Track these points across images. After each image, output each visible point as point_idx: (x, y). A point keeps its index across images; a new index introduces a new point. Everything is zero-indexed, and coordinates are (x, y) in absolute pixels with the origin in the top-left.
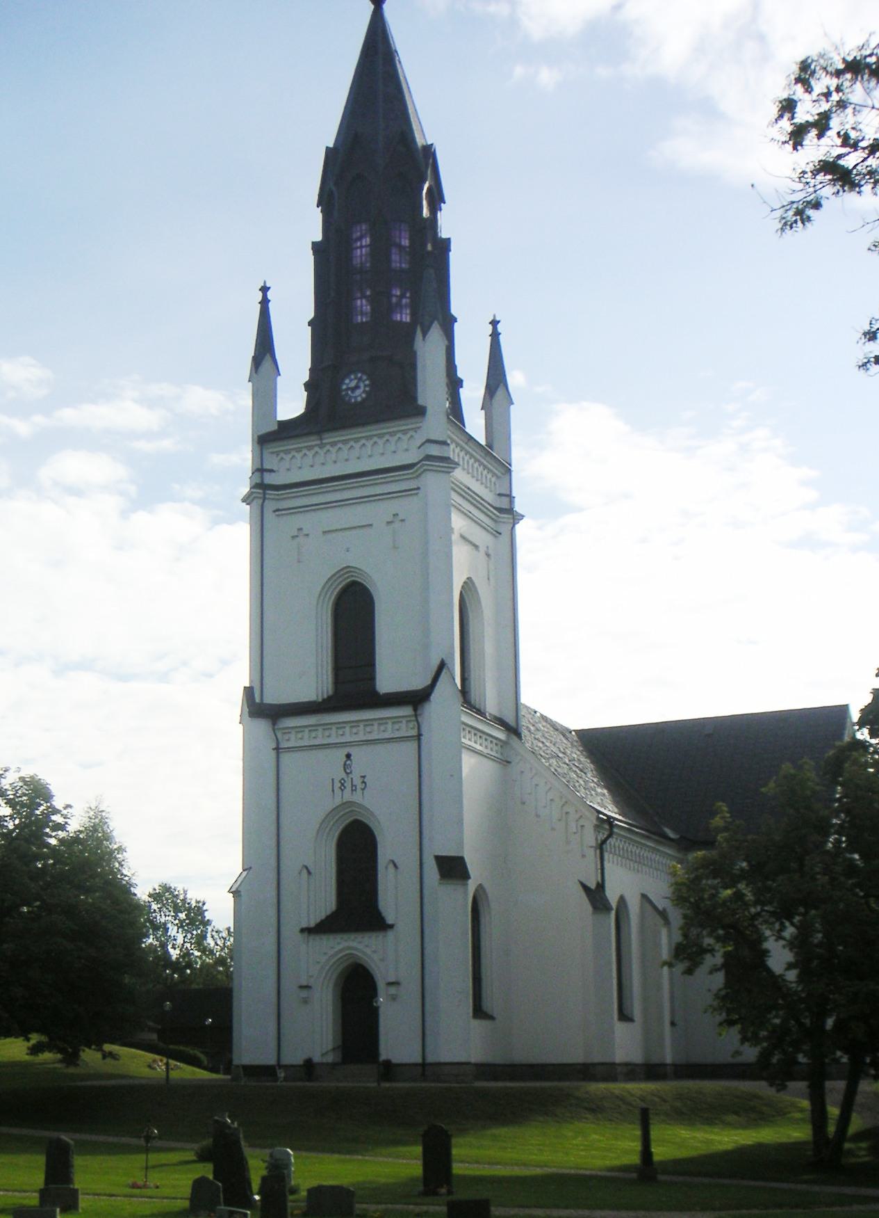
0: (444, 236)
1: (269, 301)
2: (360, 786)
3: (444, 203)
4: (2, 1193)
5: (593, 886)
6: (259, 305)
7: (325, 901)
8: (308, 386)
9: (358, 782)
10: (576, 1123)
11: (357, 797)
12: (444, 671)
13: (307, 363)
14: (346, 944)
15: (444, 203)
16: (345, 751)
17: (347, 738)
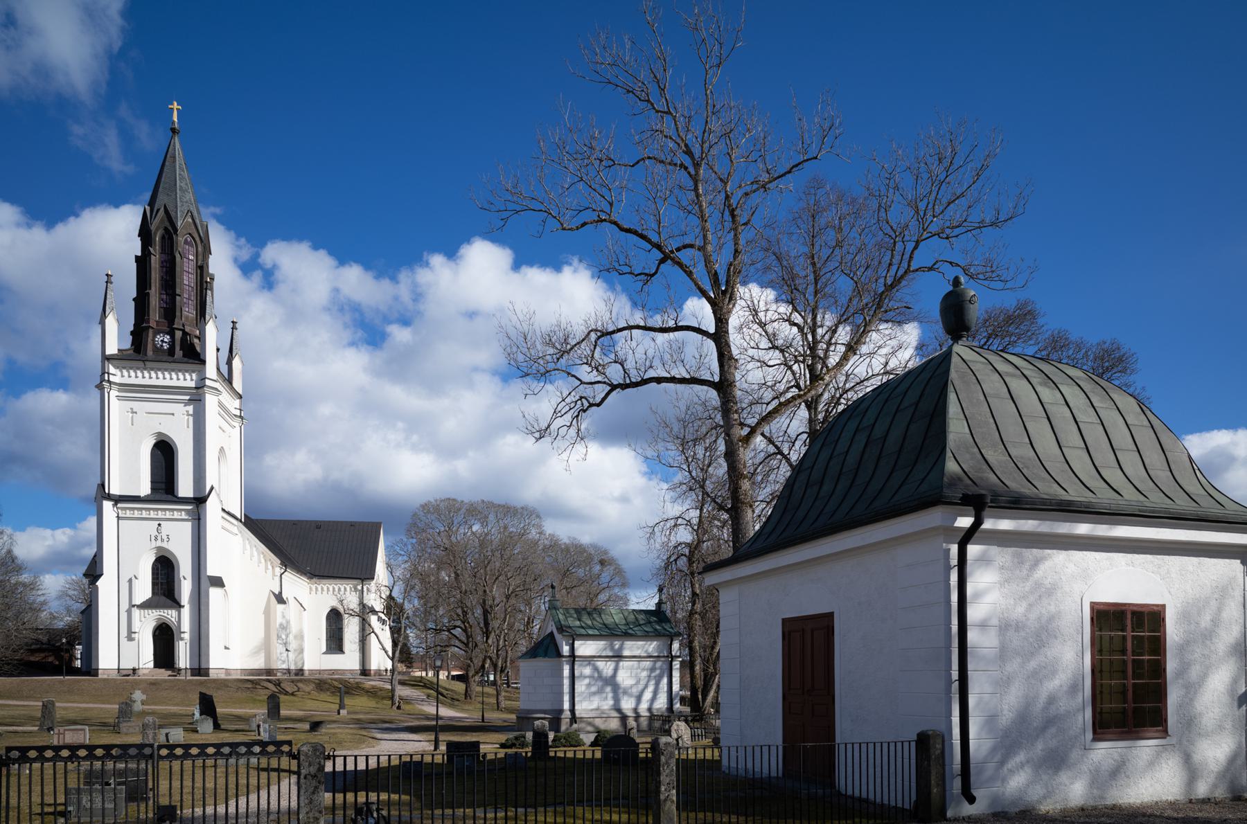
0: (116, 352)
1: (134, 300)
2: (166, 539)
3: (136, 257)
5: (277, 593)
6: (133, 302)
7: (144, 590)
8: (132, 333)
9: (165, 537)
10: (432, 500)
11: (165, 545)
12: (214, 490)
13: (133, 322)
14: (159, 613)
15: (136, 257)
16: (158, 522)
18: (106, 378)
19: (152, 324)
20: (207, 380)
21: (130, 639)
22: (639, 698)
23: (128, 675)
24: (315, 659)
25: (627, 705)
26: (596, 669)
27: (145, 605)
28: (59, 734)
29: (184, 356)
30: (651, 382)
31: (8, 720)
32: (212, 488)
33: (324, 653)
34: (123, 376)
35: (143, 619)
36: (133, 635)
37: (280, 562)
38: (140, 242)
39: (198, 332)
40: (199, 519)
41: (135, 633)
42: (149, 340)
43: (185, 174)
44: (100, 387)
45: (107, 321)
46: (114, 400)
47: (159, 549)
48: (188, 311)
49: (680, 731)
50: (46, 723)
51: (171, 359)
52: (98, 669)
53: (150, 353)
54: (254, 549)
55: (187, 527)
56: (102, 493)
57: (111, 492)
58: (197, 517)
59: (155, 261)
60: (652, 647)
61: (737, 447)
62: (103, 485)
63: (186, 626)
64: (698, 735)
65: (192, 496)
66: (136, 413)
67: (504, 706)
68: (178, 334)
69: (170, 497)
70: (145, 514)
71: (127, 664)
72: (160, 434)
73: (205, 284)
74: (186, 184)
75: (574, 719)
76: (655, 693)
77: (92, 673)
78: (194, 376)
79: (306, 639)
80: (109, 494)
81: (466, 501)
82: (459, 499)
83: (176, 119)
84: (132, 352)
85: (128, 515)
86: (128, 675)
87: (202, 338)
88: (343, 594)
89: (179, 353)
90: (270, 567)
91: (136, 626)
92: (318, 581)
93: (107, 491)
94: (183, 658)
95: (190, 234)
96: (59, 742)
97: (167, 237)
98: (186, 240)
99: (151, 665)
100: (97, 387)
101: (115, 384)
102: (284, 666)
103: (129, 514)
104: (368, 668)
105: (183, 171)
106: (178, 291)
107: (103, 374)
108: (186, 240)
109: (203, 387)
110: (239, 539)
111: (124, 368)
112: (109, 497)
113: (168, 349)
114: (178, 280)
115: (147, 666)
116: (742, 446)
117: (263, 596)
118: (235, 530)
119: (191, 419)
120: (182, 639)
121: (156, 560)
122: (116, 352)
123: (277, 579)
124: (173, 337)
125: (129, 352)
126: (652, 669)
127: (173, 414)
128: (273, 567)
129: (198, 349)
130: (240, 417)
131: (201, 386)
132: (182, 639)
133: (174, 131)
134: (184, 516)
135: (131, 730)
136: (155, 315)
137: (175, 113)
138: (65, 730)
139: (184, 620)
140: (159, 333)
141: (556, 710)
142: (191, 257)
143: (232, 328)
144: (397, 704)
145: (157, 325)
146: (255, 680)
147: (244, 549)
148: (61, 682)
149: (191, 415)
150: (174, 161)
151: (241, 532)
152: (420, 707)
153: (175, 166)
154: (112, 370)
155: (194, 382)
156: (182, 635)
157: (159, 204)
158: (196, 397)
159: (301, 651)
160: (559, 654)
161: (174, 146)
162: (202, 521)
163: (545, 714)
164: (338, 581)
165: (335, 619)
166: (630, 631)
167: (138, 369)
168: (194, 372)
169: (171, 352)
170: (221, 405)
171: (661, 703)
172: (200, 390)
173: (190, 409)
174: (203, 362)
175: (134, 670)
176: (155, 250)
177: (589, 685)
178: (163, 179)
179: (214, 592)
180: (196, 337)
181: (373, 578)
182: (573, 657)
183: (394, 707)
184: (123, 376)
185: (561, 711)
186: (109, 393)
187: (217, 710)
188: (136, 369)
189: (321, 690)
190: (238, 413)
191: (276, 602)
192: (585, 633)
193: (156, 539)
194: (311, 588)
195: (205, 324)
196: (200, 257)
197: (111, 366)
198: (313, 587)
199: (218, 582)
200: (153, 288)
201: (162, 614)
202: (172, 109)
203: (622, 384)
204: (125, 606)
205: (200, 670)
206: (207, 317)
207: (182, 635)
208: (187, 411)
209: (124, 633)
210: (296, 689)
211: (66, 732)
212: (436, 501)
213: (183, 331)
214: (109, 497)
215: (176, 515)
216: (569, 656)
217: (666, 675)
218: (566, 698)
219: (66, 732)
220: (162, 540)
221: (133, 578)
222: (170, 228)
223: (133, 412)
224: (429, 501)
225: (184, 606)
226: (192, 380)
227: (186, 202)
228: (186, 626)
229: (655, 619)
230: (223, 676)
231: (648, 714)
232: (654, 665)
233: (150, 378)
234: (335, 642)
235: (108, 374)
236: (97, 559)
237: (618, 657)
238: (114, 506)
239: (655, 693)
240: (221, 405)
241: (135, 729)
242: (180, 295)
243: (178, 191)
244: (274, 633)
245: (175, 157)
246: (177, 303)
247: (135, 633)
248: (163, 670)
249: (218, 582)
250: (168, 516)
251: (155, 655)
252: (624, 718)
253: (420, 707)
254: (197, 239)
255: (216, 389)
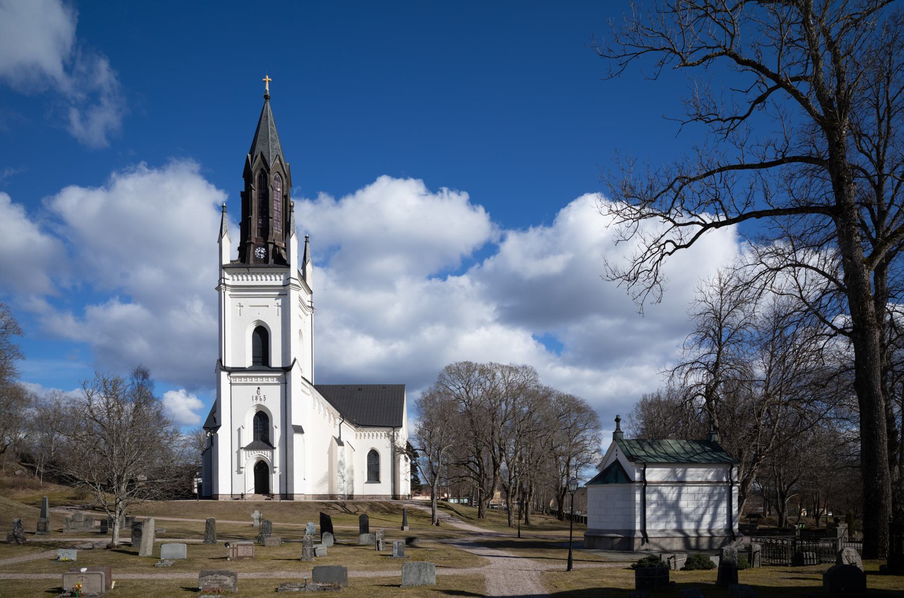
0: (229, 262)
2: (263, 399)
3: (242, 192)
4: (1, 583)
5: (337, 438)
7: (248, 437)
8: (239, 249)
9: (262, 397)
10: (453, 364)
11: (262, 403)
14: (259, 453)
15: (242, 192)
16: (258, 386)
17: (259, 382)
18: (223, 282)
19: (253, 241)
20: (291, 279)
21: (239, 472)
22: (699, 522)
23: (238, 499)
24: (362, 488)
25: (689, 527)
26: (660, 494)
27: (250, 448)
28: (233, 548)
29: (275, 263)
30: (750, 217)
31: (175, 533)
32: (295, 360)
33: (366, 483)
34: (233, 280)
35: (248, 458)
36: (241, 470)
37: (339, 414)
38: (244, 181)
39: (284, 245)
40: (286, 383)
41: (243, 468)
42: (251, 252)
43: (274, 129)
44: (219, 289)
45: (223, 240)
46: (228, 298)
47: (259, 406)
48: (277, 229)
49: (851, 558)
50: (209, 537)
51: (266, 265)
52: (293, 494)
53: (252, 262)
54: (321, 405)
55: (277, 390)
56: (221, 366)
57: (226, 365)
58: (284, 382)
59: (255, 194)
60: (709, 474)
61: (861, 269)
62: (221, 361)
63: (277, 463)
64: (810, 558)
65: (280, 366)
66: (242, 306)
67: (514, 523)
68: (271, 247)
69: (266, 368)
70: (249, 381)
71: (238, 491)
72: (259, 321)
73: (288, 207)
74: (275, 136)
75: (645, 538)
76: (714, 516)
77: (214, 497)
78: (282, 277)
79: (355, 472)
80: (225, 366)
81: (479, 364)
82: (474, 362)
83: (267, 89)
84: (239, 262)
85: (237, 382)
86: (238, 499)
87: (287, 249)
88: (379, 440)
89: (271, 261)
90: (332, 419)
91: (243, 463)
92: (361, 429)
93: (223, 365)
94: (275, 487)
95: (278, 172)
96: (233, 556)
97: (262, 176)
98: (276, 176)
99: (253, 491)
100: (216, 289)
101: (229, 286)
102: (342, 493)
103: (238, 381)
104: (397, 494)
105: (273, 126)
106: (270, 215)
107: (220, 279)
108: (275, 177)
109: (289, 284)
110: (311, 398)
111: (235, 274)
112: (225, 369)
113: (264, 258)
114: (270, 207)
115: (250, 492)
116: (867, 268)
117: (328, 440)
118: (308, 391)
119: (280, 308)
120: (275, 472)
121: (256, 414)
122: (229, 262)
123: (338, 427)
124: (267, 249)
125: (237, 262)
126: (711, 495)
127: (268, 306)
128: (334, 418)
129: (285, 257)
130: (312, 307)
131: (287, 284)
132: (275, 472)
133: (266, 97)
134: (276, 382)
135: (273, 544)
136: (255, 234)
137: (267, 83)
138: (238, 545)
139: (275, 458)
140: (257, 247)
141: (626, 531)
142: (279, 189)
143: (306, 242)
144: (436, 522)
145: (256, 241)
146: (328, 502)
147: (314, 405)
148: (196, 504)
149: (280, 306)
150: (267, 120)
151: (312, 393)
152: (450, 524)
153: (267, 123)
154: (227, 276)
155: (282, 281)
156: (275, 470)
157: (257, 152)
158: (284, 293)
159: (352, 482)
160: (629, 480)
161: (267, 108)
162: (288, 385)
163: (617, 534)
164: (376, 429)
165: (374, 456)
166: (692, 459)
167: (244, 274)
168: (282, 274)
169: (266, 260)
170: (301, 299)
171: (721, 523)
172: (287, 287)
173: (279, 301)
174: (289, 266)
175: (242, 495)
176: (254, 186)
177: (655, 511)
178: (259, 133)
179: (297, 437)
180: (283, 248)
181: (401, 426)
182: (643, 480)
183: (434, 524)
184: (233, 280)
185: (634, 531)
186: (224, 293)
187: (334, 527)
188: (242, 274)
189: (374, 510)
190: (309, 304)
191: (337, 444)
192: (655, 461)
193: (256, 399)
194: (356, 435)
195: (290, 237)
196: (285, 189)
197: (226, 273)
198: (359, 434)
199: (299, 430)
200: (253, 214)
201: (260, 454)
202: (265, 81)
203: (717, 223)
204: (236, 448)
205: (287, 495)
206: (291, 232)
207: (275, 470)
208: (278, 304)
209: (235, 468)
210: (356, 510)
211: (239, 547)
212: (456, 364)
213: (274, 244)
214: (225, 369)
215: (270, 381)
216: (641, 482)
217: (725, 498)
218: (638, 519)
219: (239, 547)
220: (261, 400)
221: (241, 428)
222: (265, 169)
223: (240, 306)
224: (451, 364)
225: (275, 448)
226: (281, 280)
227: (276, 149)
228: (277, 463)
229: (709, 448)
230: (303, 500)
231: (708, 535)
232: (713, 491)
233: (257, 280)
234: (374, 475)
235: (224, 278)
236: (216, 415)
237: (681, 483)
238: (228, 375)
239: (714, 516)
240: (301, 299)
241: (276, 543)
242: (271, 218)
243: (270, 141)
244: (334, 466)
245: (267, 117)
246: (270, 224)
247: (243, 468)
248: (261, 495)
249: (299, 430)
250: (264, 382)
251: (255, 484)
252: (686, 538)
253: (450, 524)
254: (283, 176)
255: (297, 286)
